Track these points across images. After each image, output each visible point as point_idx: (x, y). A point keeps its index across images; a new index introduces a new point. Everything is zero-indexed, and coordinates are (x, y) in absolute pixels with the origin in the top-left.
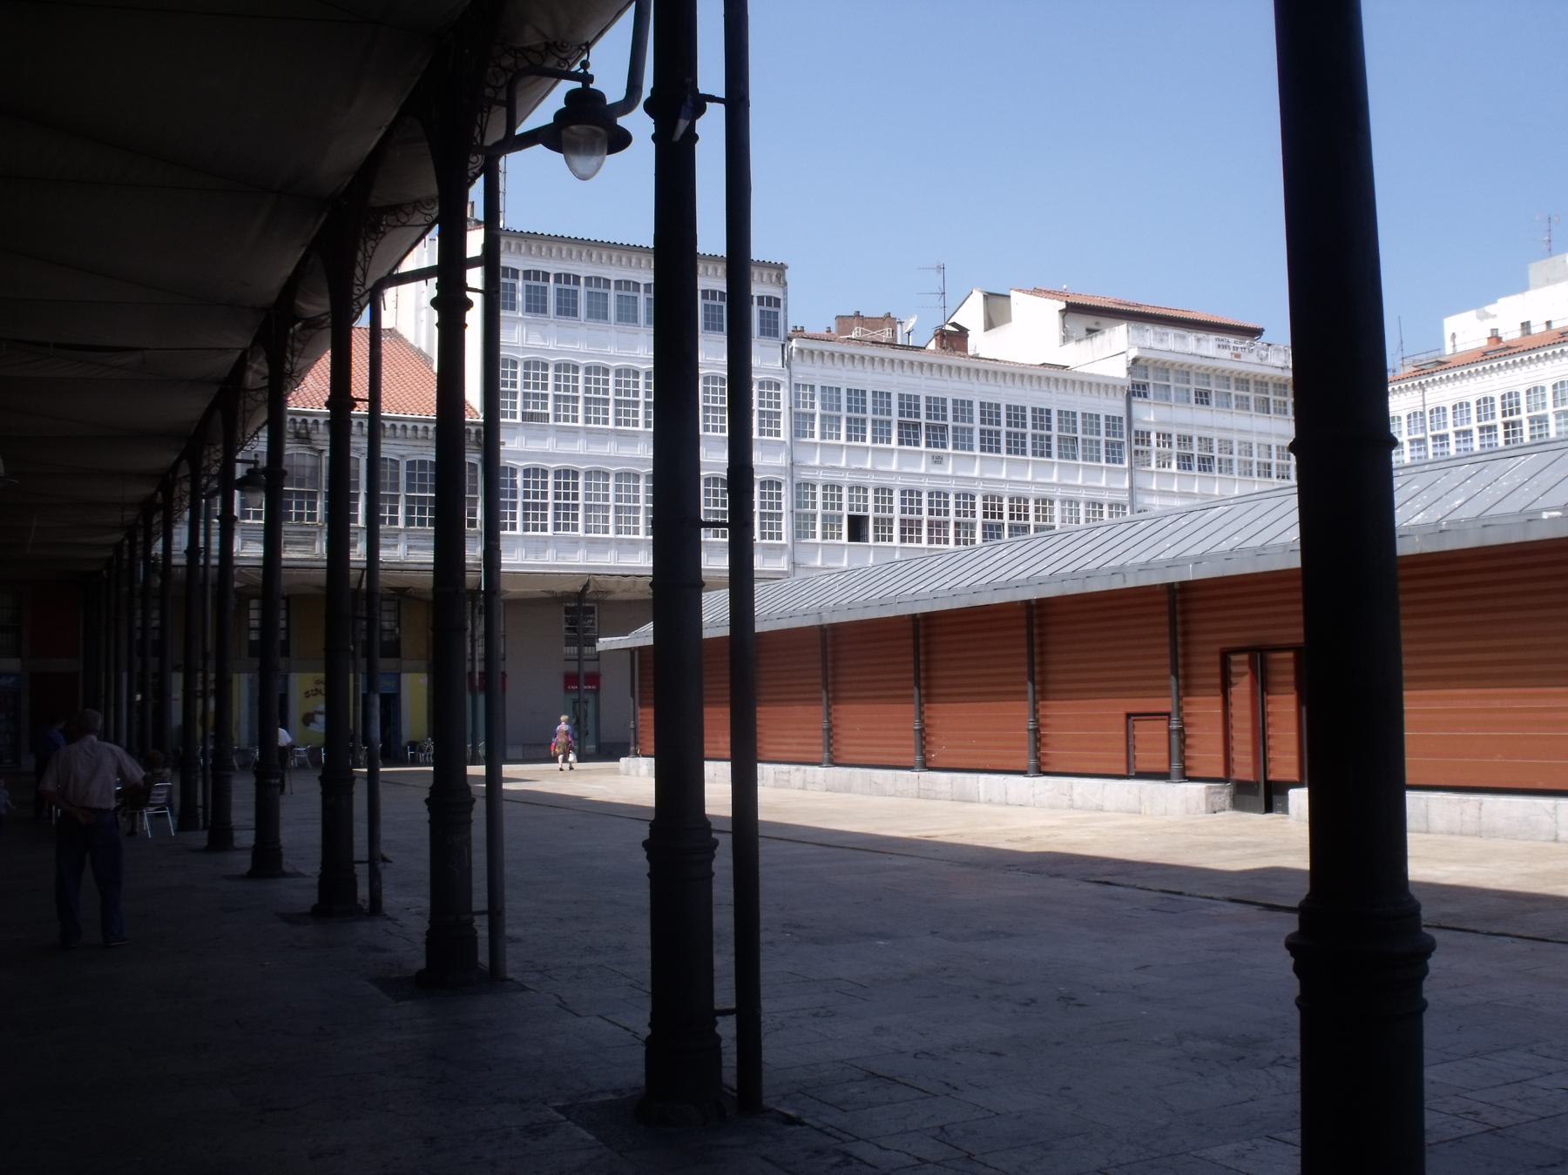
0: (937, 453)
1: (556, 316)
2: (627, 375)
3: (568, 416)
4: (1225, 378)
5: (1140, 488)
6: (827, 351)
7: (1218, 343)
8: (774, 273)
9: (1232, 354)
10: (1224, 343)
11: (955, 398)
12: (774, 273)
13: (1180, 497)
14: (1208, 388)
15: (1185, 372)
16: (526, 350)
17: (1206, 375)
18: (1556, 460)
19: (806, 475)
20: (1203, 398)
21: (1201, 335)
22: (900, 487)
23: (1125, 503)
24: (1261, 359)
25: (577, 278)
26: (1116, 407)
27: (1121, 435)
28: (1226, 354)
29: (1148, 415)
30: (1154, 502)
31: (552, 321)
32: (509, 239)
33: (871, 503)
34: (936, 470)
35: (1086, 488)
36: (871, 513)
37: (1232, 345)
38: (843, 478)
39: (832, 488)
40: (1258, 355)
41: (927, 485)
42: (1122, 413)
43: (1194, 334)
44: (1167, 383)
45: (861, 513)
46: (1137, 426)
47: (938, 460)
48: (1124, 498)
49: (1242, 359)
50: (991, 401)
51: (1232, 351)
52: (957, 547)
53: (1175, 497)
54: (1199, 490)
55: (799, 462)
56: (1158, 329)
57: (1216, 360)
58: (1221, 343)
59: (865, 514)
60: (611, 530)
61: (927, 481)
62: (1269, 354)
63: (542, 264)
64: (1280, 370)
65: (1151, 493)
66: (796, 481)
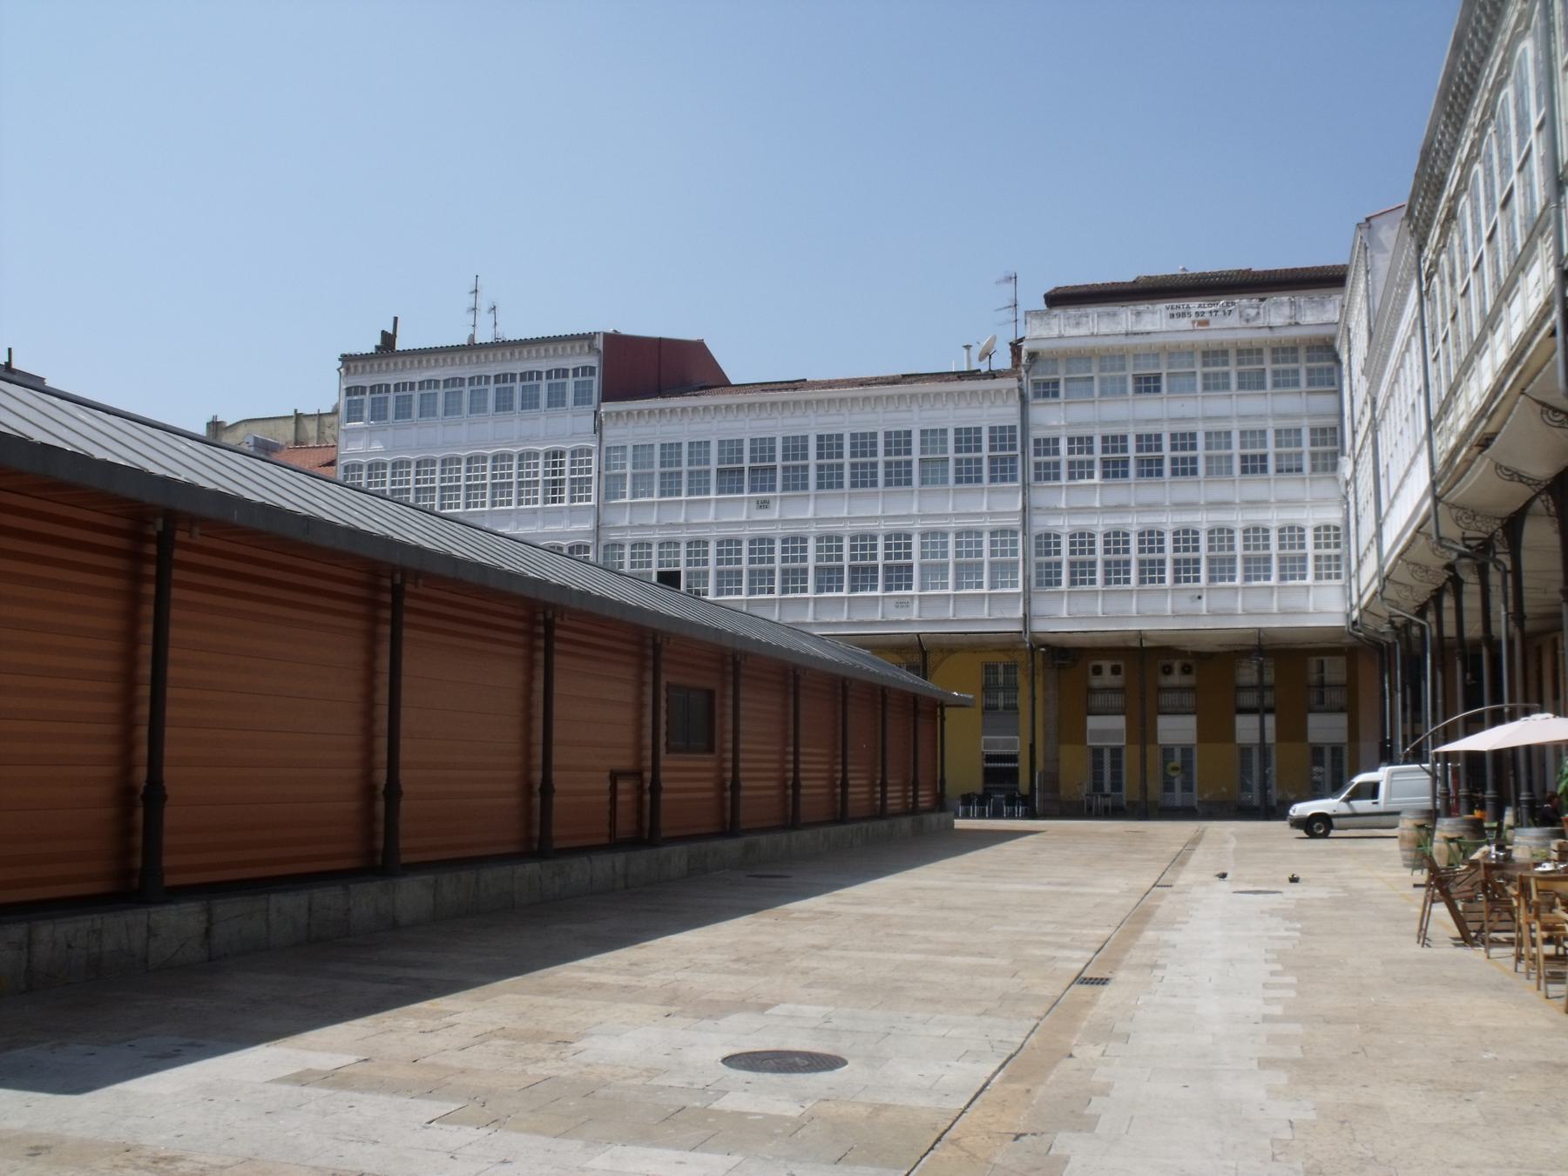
0: (762, 497)
1: (495, 413)
2: (401, 467)
3: (1177, 469)
4: (1175, 353)
5: (1038, 508)
6: (656, 409)
7: (1170, 311)
8: (586, 344)
9: (1193, 322)
10: (1181, 311)
11: (691, 441)
12: (586, 344)
13: (1069, 514)
14: (1054, 377)
15: (1111, 357)
16: (367, 454)
17: (1155, 353)
18: (233, 481)
19: (615, 536)
20: (1148, 384)
21: (1142, 307)
22: (920, 531)
23: (1015, 528)
24: (1247, 321)
25: (388, 386)
26: (1007, 414)
27: (1013, 447)
28: (1185, 323)
29: (1051, 418)
30: (1270, 517)
31: (391, 426)
32: (355, 363)
33: (683, 558)
34: (761, 515)
35: (719, 525)
36: (683, 568)
37: (1193, 311)
38: (625, 536)
39: (641, 546)
40: (1241, 316)
41: (953, 525)
42: (1017, 422)
43: (1132, 307)
44: (1192, 370)
45: (672, 569)
46: (1036, 433)
47: (764, 504)
48: (1015, 522)
49: (1212, 326)
50: (830, 432)
51: (1193, 317)
52: (1343, 576)
53: (1095, 513)
54: (1101, 502)
55: (609, 524)
56: (1072, 311)
57: (1153, 335)
58: (1175, 312)
59: (676, 569)
60: (986, 584)
61: (629, 533)
62: (1261, 311)
63: (384, 378)
64: (1267, 330)
65: (1056, 512)
66: (603, 542)
